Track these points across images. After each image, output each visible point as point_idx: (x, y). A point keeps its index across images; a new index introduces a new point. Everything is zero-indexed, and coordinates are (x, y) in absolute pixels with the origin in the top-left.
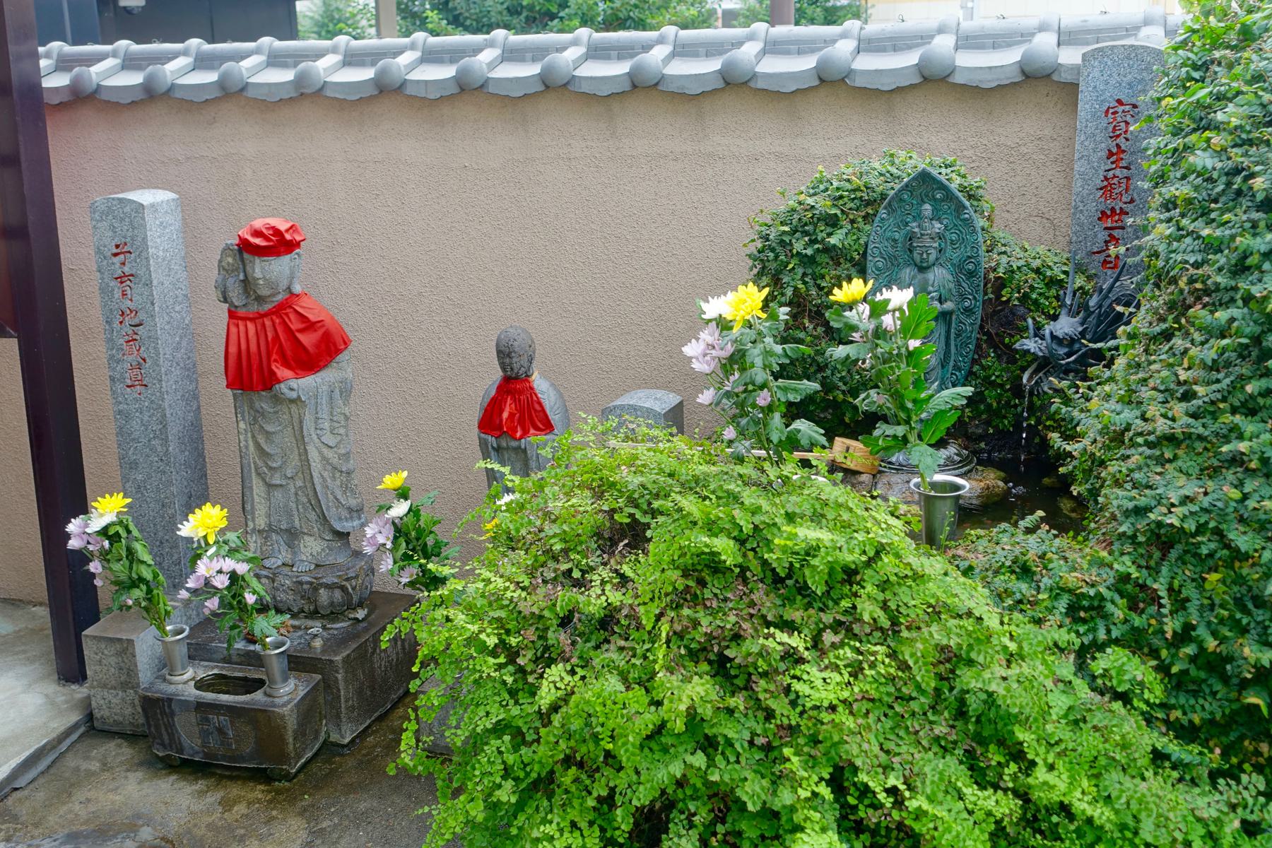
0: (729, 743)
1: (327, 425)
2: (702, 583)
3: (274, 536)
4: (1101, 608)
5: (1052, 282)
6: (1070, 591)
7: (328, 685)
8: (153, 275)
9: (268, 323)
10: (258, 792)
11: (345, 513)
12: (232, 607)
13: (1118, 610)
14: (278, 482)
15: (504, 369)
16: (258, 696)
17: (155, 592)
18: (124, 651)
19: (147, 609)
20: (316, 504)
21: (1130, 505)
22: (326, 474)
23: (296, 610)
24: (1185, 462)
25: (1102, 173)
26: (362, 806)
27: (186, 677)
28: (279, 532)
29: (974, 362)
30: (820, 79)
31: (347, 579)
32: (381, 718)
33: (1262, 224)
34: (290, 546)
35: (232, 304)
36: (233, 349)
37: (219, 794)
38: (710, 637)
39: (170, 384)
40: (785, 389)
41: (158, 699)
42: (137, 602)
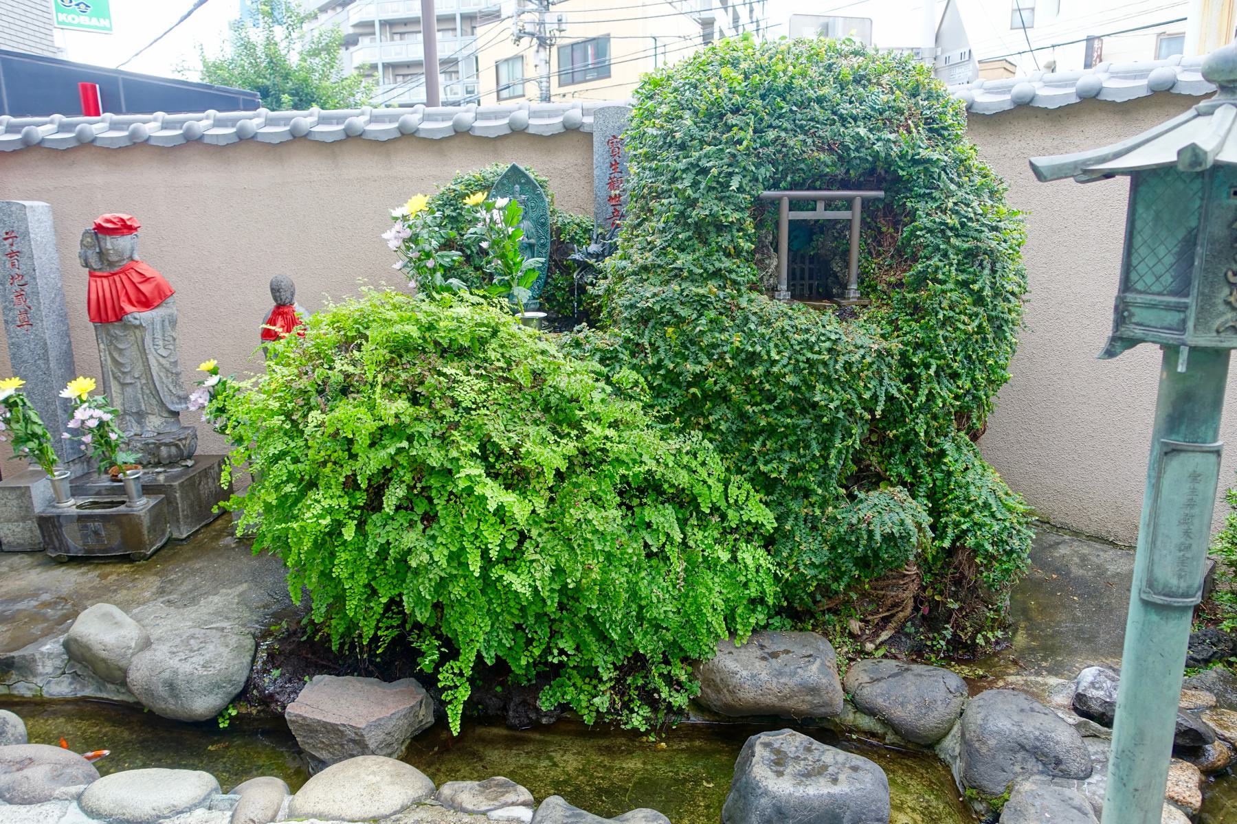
0: (420, 434)
1: (161, 343)
2: (400, 356)
3: (128, 418)
4: (616, 357)
5: (586, 231)
6: (601, 350)
7: (169, 501)
8: (34, 252)
9: (117, 278)
10: (125, 568)
11: (176, 400)
12: (101, 445)
13: (625, 356)
14: (129, 381)
15: (276, 300)
16: (122, 508)
17: (45, 445)
18: (23, 495)
19: (39, 458)
20: (156, 393)
21: (628, 303)
22: (162, 374)
23: (145, 463)
24: (653, 279)
25: (608, 176)
26: (197, 566)
27: (69, 504)
28: (132, 414)
29: (548, 277)
30: (455, 131)
31: (180, 440)
32: (207, 525)
33: (681, 156)
34: (139, 423)
35: (91, 267)
36: (94, 296)
37: (97, 572)
38: (406, 381)
39: (48, 328)
40: (442, 257)
41: (50, 517)
42: (32, 450)
